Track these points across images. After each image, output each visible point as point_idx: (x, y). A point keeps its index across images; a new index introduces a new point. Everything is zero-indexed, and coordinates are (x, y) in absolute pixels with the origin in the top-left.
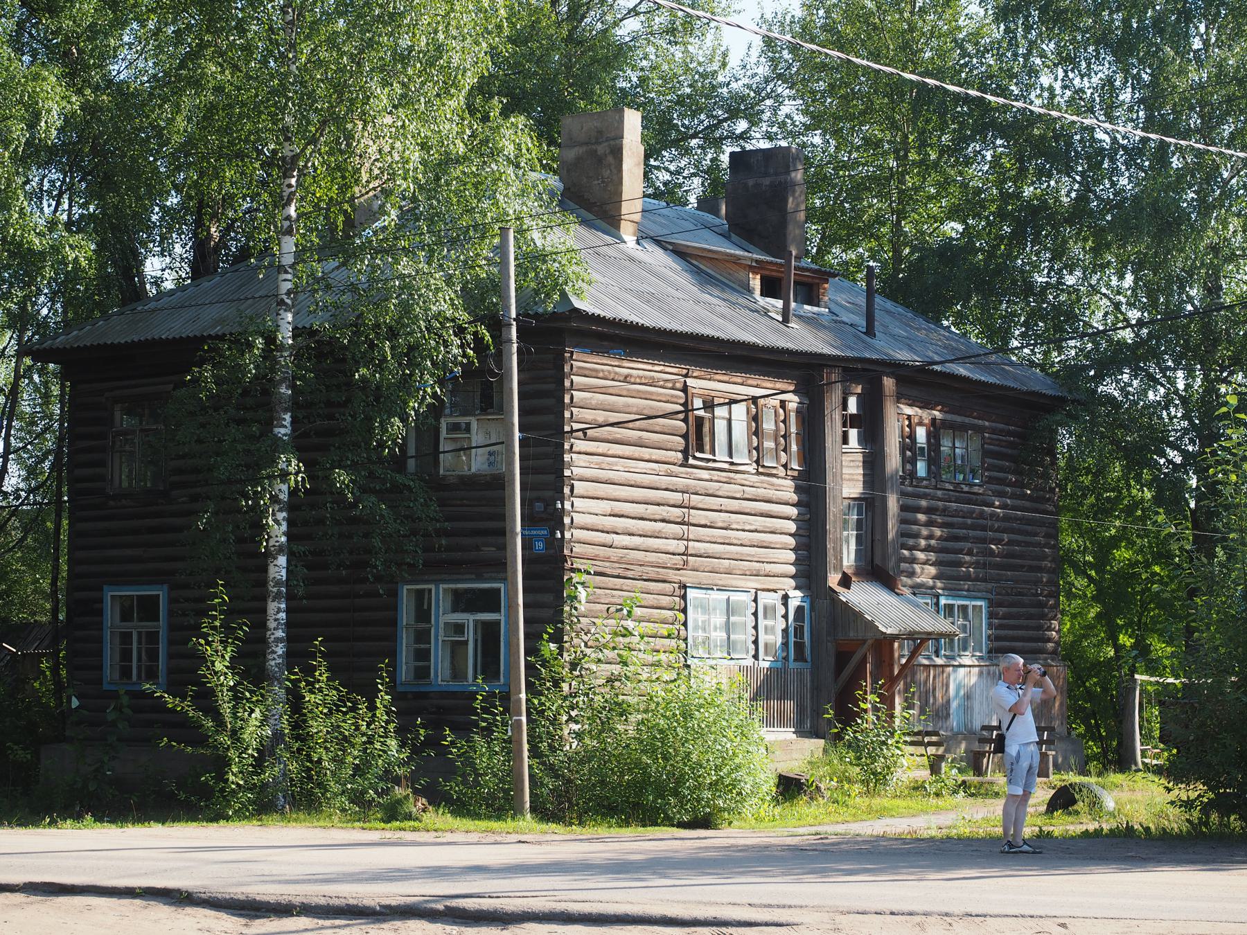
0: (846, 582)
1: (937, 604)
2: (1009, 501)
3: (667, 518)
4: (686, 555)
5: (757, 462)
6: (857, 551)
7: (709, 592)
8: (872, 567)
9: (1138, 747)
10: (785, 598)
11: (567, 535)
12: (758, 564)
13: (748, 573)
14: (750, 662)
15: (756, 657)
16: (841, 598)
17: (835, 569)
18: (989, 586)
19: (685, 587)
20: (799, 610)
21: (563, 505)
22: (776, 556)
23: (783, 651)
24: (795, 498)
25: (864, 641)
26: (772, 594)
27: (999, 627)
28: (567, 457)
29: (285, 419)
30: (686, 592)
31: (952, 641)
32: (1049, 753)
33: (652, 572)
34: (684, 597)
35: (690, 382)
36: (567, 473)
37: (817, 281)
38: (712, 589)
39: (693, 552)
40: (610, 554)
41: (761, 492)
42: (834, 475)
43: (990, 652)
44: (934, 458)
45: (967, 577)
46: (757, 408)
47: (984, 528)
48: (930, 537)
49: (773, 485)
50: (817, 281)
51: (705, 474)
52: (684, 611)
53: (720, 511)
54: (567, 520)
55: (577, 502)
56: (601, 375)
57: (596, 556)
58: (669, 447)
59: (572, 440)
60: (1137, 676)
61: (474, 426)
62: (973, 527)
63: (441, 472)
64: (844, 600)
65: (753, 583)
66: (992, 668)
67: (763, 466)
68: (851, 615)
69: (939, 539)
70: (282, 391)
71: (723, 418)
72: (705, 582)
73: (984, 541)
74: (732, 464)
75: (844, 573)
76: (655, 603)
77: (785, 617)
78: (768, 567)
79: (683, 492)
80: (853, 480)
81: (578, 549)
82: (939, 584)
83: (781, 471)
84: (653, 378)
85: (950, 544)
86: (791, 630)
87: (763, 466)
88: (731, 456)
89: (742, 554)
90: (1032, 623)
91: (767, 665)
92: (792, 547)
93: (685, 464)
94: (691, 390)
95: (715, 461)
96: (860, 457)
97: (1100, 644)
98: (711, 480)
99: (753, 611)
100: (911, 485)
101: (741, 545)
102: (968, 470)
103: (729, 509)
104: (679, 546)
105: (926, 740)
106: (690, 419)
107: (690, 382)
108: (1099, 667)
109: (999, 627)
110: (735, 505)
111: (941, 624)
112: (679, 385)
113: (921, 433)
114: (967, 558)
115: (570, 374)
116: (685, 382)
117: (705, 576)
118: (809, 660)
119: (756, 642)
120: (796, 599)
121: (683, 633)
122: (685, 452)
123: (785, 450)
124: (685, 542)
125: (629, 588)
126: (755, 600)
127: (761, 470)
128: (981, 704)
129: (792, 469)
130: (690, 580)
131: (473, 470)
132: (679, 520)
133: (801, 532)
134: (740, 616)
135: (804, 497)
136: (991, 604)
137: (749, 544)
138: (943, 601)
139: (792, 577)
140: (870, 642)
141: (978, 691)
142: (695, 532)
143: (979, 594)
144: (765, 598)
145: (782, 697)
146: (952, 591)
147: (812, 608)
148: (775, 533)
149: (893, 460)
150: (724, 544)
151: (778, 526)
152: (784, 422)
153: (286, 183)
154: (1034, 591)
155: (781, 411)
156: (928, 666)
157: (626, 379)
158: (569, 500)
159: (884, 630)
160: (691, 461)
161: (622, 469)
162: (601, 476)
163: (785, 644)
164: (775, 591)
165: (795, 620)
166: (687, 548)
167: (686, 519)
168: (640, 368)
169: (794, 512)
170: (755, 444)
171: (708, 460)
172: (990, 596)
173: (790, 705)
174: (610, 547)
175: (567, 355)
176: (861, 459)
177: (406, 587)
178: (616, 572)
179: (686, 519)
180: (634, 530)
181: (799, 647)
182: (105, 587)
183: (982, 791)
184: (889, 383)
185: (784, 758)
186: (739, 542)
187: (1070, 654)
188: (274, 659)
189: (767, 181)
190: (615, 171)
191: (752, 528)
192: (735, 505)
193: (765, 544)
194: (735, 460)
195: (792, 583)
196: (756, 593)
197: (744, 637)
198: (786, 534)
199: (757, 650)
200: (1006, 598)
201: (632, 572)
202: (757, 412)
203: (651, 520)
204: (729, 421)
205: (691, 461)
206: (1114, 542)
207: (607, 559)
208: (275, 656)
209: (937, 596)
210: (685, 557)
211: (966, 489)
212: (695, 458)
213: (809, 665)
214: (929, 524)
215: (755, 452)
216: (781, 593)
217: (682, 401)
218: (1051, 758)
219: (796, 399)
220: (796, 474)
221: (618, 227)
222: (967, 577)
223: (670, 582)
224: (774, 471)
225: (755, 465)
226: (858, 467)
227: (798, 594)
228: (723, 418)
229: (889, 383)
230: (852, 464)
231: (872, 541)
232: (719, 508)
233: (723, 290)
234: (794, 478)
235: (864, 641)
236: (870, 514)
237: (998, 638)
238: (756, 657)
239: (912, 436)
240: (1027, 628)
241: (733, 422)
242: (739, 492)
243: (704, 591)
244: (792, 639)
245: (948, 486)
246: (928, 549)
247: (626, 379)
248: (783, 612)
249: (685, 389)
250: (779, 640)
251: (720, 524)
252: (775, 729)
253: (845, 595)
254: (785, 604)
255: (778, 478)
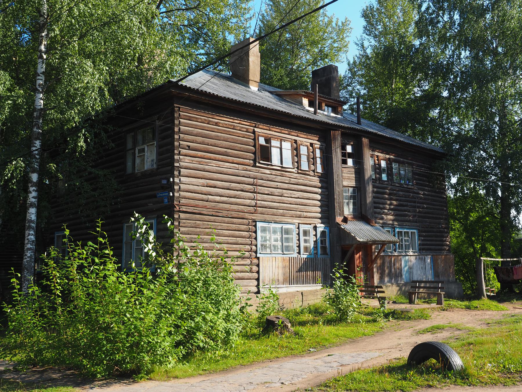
0: (345, 220)
1: (394, 231)
2: (426, 192)
3: (244, 190)
4: (256, 207)
5: (298, 168)
6: (353, 208)
7: (270, 224)
8: (361, 215)
9: (484, 288)
10: (315, 228)
11: (176, 194)
12: (300, 212)
13: (294, 216)
14: (295, 255)
15: (299, 253)
16: (342, 227)
17: (340, 215)
18: (418, 224)
19: (256, 222)
20: (323, 233)
21: (173, 180)
22: (310, 209)
23: (314, 250)
24: (320, 185)
25: (352, 245)
26: (309, 226)
27: (422, 240)
28: (176, 157)
29: (36, 143)
30: (256, 224)
31: (395, 245)
32: (442, 293)
33: (234, 214)
34: (255, 226)
35: (256, 129)
36: (176, 164)
37: (337, 105)
38: (272, 222)
39: (259, 205)
40: (207, 204)
41: (301, 181)
42: (338, 175)
43: (420, 250)
44: (390, 174)
45: (409, 221)
46: (297, 145)
47: (415, 202)
48: (391, 204)
49: (307, 178)
50: (337, 105)
51: (268, 171)
52: (255, 232)
53: (278, 188)
54: (176, 187)
55: (183, 179)
56: (200, 120)
57: (197, 205)
58: (245, 157)
59: (180, 149)
60: (482, 258)
61: (146, 149)
62: (410, 202)
63: (136, 172)
64: (343, 228)
65: (297, 221)
66: (421, 256)
67: (301, 170)
68: (346, 234)
69: (396, 205)
70: (34, 130)
71: (277, 147)
72: (268, 219)
73: (415, 207)
74: (282, 167)
75: (345, 217)
76: (237, 228)
77: (316, 235)
78: (305, 214)
79: (254, 179)
80: (350, 179)
81: (183, 201)
82: (396, 223)
83: (312, 173)
84: (234, 126)
85: (399, 208)
86: (319, 241)
87: (301, 170)
88: (282, 163)
89: (290, 208)
90: (439, 239)
91: (305, 256)
92: (319, 206)
93: (254, 166)
94: (257, 134)
95: (272, 165)
96: (353, 170)
97: (468, 248)
98: (272, 174)
99: (297, 233)
100: (380, 183)
101: (290, 204)
102: (406, 179)
103: (282, 187)
104: (253, 203)
105: (376, 290)
106: (257, 146)
107: (256, 129)
108: (467, 255)
109: (422, 240)
110: (286, 186)
111: (390, 238)
112: (252, 131)
113: (383, 164)
114: (409, 213)
115: (178, 118)
116: (254, 129)
117: (268, 217)
118: (329, 254)
119: (299, 247)
120: (321, 227)
121: (254, 242)
122: (255, 161)
123: (313, 164)
124: (256, 201)
125: (219, 221)
126: (298, 228)
127: (299, 171)
128: (417, 271)
129: (317, 172)
130: (258, 218)
131: (146, 169)
132: (252, 191)
133: (324, 199)
134: (291, 235)
135: (325, 185)
136: (419, 231)
137: (294, 203)
138: (397, 230)
139: (320, 218)
140: (355, 246)
141: (415, 266)
142: (259, 196)
143: (414, 227)
144: (303, 227)
145: (314, 269)
146: (401, 226)
147: (330, 231)
148: (310, 199)
149: (369, 172)
150: (280, 203)
151: (311, 196)
152: (313, 152)
153: (40, 35)
154: (438, 227)
155: (311, 148)
156: (391, 256)
157: (217, 124)
158: (178, 177)
159: (361, 240)
160: (257, 164)
161: (215, 165)
162: (199, 167)
163: (315, 247)
164: (310, 224)
165: (321, 237)
166: (256, 203)
167: (256, 190)
168: (225, 120)
169: (320, 190)
170: (297, 160)
171: (268, 165)
172: (418, 228)
173: (319, 274)
174: (207, 201)
175: (176, 109)
176: (354, 171)
177: (126, 225)
178: (211, 213)
179: (256, 190)
180: (223, 194)
181: (324, 248)
182: (56, 232)
183: (403, 316)
184: (365, 141)
185: (313, 298)
186: (289, 202)
187: (456, 251)
188: (26, 258)
189: (324, 78)
190: (247, 62)
191: (296, 196)
192: (286, 186)
193: (303, 204)
194: (284, 166)
195: (320, 221)
196: (299, 225)
197: (294, 244)
198: (316, 200)
199: (300, 250)
200: (426, 229)
201: (221, 214)
202: (297, 147)
203: (234, 190)
204: (281, 149)
205: (257, 164)
206: (470, 211)
207: (205, 207)
208: (26, 257)
209: (394, 228)
210: (255, 208)
211: (406, 186)
212: (260, 163)
213: (329, 256)
214: (391, 199)
215: (296, 164)
216: (313, 226)
217: (253, 138)
218: (443, 295)
219: (319, 143)
220: (320, 175)
221: (248, 83)
222: (409, 221)
223: (247, 219)
224: (307, 173)
225: (296, 169)
226: (352, 174)
227: (322, 225)
228: (277, 147)
229: (365, 141)
230: (349, 172)
231: (361, 204)
232: (276, 187)
233: (285, 102)
234: (319, 177)
235: (352, 245)
236: (359, 194)
237: (423, 245)
238: (299, 253)
239: (379, 165)
240: (436, 241)
241: (283, 150)
242: (288, 180)
243: (268, 224)
244: (319, 245)
245: (397, 185)
246: (390, 209)
247: (217, 124)
248: (314, 233)
249: (254, 132)
250: (312, 246)
251: (277, 194)
252: (311, 285)
253: (343, 226)
254: (316, 230)
255: (310, 176)
